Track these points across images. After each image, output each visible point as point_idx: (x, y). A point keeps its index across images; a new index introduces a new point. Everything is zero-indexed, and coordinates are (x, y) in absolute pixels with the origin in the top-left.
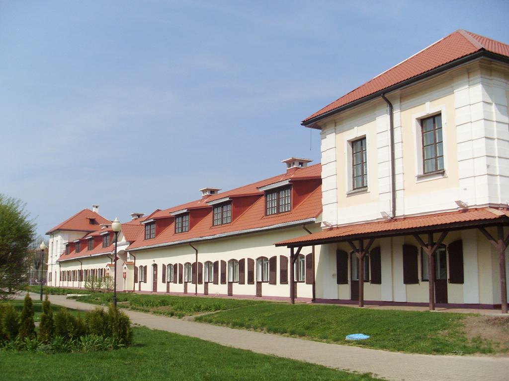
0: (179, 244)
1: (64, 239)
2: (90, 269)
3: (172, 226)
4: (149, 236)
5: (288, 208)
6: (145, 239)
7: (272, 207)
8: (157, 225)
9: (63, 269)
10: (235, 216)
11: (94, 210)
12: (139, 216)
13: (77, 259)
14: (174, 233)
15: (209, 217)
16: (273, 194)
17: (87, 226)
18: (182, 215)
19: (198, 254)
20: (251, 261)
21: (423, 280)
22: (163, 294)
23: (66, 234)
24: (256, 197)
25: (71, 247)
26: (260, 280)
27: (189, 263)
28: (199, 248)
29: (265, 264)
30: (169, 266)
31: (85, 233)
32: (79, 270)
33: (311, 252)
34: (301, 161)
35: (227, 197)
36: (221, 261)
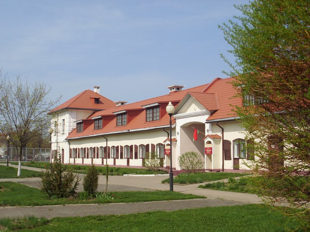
0: (78, 138)
1: (73, 118)
2: (80, 148)
3: (93, 125)
4: (79, 130)
5: (158, 118)
6: (117, 126)
7: (156, 116)
8: (84, 124)
9: (73, 146)
10: (104, 125)
11: (95, 90)
12: (178, 88)
13: (103, 135)
14: (115, 126)
15: (115, 120)
16: (157, 109)
17: (92, 105)
18: (122, 114)
19: (108, 142)
20: (136, 146)
21: (100, 158)
22: (230, 172)
23: (74, 113)
24: (142, 110)
25: (84, 124)
26: (236, 157)
27: (74, 148)
28: (108, 139)
29: (161, 148)
30: (113, 147)
31: (90, 113)
32: (55, 150)
33: (106, 146)
34: (178, 87)
35: (124, 110)
36: (135, 145)
